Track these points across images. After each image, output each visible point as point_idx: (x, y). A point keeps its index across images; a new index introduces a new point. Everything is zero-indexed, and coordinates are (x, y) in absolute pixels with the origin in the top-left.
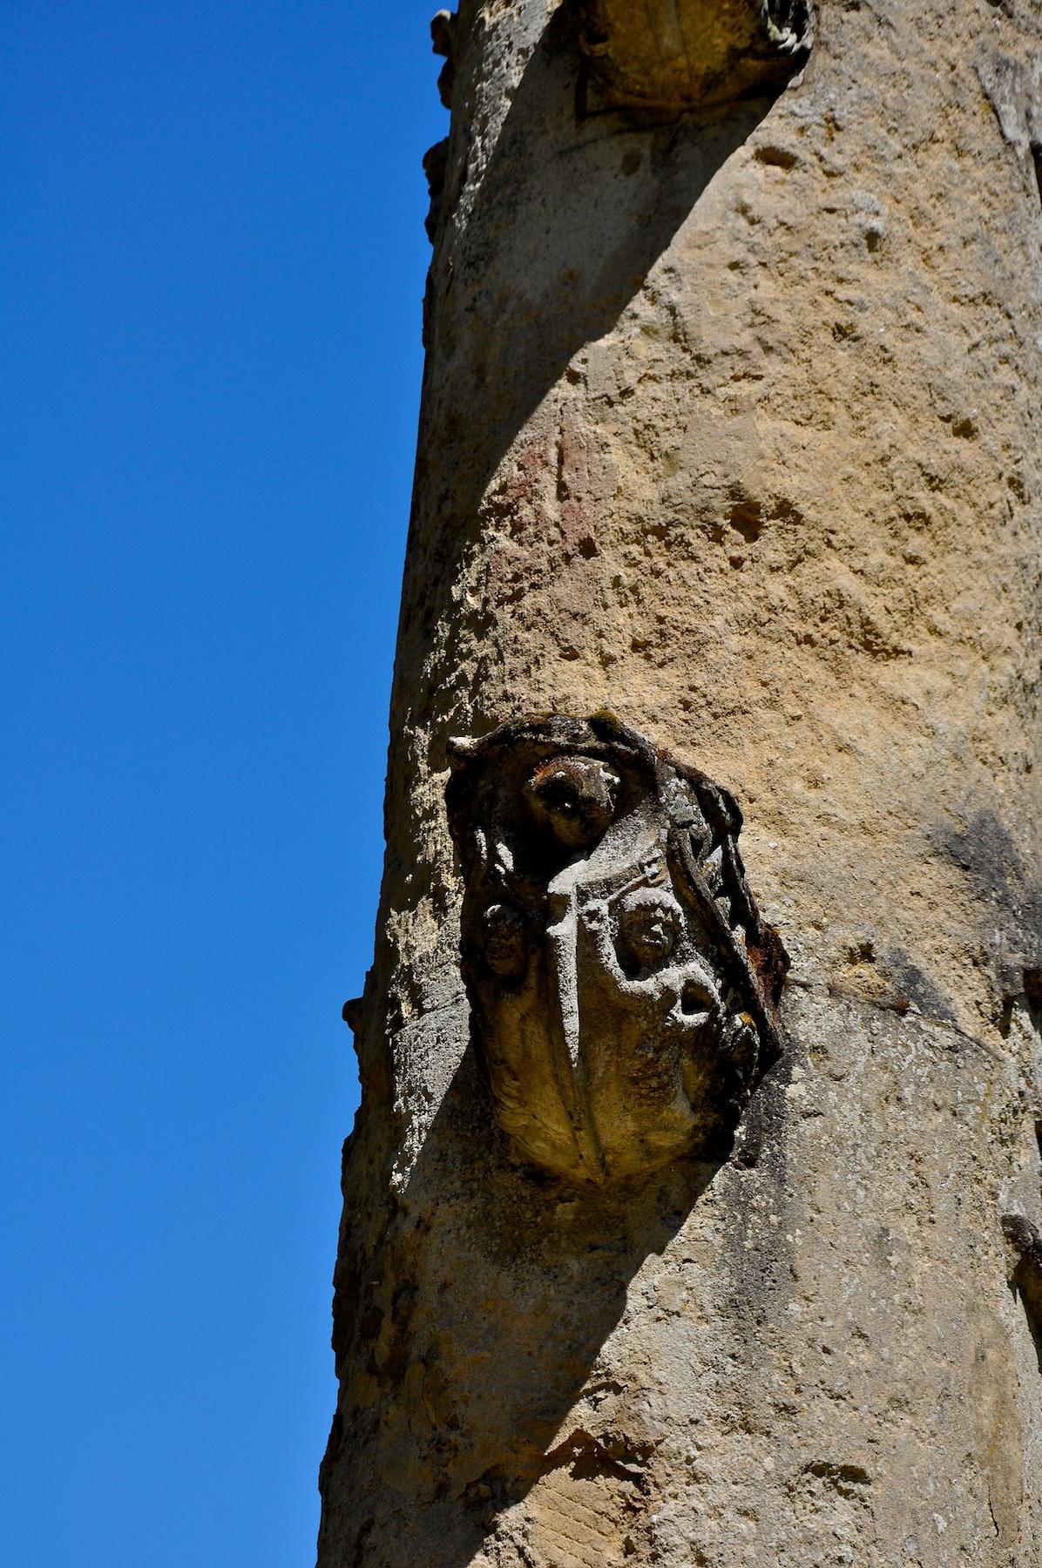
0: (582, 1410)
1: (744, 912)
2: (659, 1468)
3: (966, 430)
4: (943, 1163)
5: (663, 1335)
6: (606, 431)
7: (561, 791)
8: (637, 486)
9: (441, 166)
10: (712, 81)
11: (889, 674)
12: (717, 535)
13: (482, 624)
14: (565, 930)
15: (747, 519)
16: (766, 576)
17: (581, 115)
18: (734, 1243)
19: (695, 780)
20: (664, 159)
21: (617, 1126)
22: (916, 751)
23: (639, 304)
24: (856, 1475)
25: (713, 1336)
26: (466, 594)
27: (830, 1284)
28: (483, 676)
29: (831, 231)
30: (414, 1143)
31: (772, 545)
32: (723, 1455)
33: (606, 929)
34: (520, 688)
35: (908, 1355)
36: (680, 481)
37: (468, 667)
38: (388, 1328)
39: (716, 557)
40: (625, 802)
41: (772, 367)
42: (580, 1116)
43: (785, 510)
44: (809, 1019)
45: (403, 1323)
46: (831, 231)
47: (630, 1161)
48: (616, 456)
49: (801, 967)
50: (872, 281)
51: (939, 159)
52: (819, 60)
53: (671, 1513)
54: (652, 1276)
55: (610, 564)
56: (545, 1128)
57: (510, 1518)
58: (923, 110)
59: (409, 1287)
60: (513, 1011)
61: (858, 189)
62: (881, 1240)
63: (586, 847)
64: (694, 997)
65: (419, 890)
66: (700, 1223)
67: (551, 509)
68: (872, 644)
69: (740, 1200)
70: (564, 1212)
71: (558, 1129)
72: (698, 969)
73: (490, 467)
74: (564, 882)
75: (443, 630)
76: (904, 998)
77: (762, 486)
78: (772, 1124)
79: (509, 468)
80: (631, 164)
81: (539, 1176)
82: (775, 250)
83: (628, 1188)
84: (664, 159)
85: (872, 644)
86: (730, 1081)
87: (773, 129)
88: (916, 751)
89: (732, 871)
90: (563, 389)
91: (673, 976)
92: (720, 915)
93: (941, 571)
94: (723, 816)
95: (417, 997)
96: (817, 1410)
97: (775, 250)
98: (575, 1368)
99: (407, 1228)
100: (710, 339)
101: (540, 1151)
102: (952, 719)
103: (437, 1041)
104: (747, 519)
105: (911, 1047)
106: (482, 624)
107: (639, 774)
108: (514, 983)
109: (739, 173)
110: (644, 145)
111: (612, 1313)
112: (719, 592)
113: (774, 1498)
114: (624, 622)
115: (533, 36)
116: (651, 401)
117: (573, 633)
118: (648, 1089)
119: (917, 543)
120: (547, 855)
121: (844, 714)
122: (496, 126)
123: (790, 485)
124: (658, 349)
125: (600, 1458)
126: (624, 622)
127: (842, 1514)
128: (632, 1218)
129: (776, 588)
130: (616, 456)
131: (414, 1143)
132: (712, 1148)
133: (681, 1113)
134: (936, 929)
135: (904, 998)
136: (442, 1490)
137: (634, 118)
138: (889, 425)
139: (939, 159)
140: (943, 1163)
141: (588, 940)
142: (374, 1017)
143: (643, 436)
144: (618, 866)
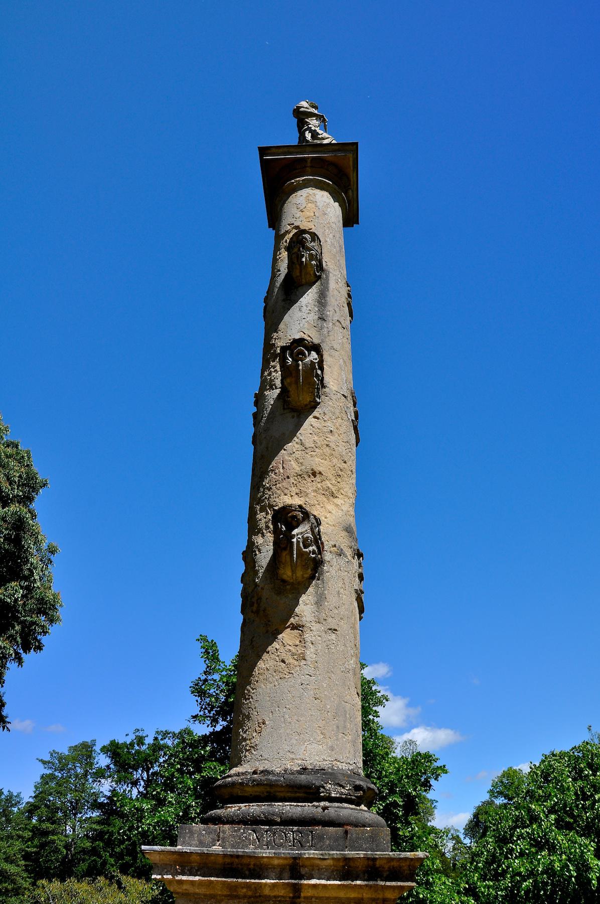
0: (292, 619)
1: (320, 539)
2: (305, 629)
3: (345, 462)
4: (347, 581)
5: (305, 607)
6: (290, 458)
7: (295, 517)
8: (295, 467)
9: (256, 417)
10: (306, 405)
11: (336, 500)
12: (309, 476)
13: (269, 489)
14: (294, 540)
15: (314, 474)
16: (317, 483)
17: (284, 409)
18: (316, 593)
19: (315, 516)
20: (299, 416)
21: (299, 573)
22: (340, 513)
23: (295, 439)
24: (336, 630)
25: (314, 608)
26: (266, 483)
27: (332, 600)
28: (270, 497)
29: (325, 430)
30: (260, 575)
31: (318, 479)
32: (315, 627)
33: (301, 540)
34: (277, 500)
35: (342, 611)
36: (303, 467)
37: (267, 496)
38: (256, 605)
39: (309, 480)
40: (304, 520)
41: (317, 450)
42: (293, 572)
43: (320, 473)
44: (327, 556)
45: (259, 605)
46: (325, 430)
47: (300, 579)
48: (292, 463)
49: (326, 548)
50: (332, 438)
51: (340, 420)
52: (322, 404)
53: (307, 636)
54: (303, 598)
55: (292, 480)
56: (286, 573)
57: (280, 636)
58: (337, 411)
59: (260, 599)
60: (284, 554)
61: (329, 424)
62: (339, 593)
63: (297, 527)
64: (314, 552)
65: (258, 532)
66: (311, 589)
67: (282, 471)
68: (333, 495)
69: (317, 586)
70: (288, 587)
71: (289, 573)
72: (314, 547)
73: (270, 464)
74: (295, 532)
75: (262, 490)
76: (340, 554)
77: (318, 469)
78: (322, 574)
79: (273, 464)
80: (293, 417)
81: (284, 581)
82: (318, 432)
83: (299, 583)
84: (299, 416)
85: (333, 495)
86: (315, 566)
87: (315, 413)
88: (340, 513)
89: (319, 531)
90: (283, 451)
91: (311, 548)
92: (317, 540)
93: (343, 485)
94: (319, 523)
95: (259, 551)
96: (330, 620)
97: (318, 432)
98: (290, 612)
99: (259, 589)
100: (307, 445)
101: (285, 577)
102: (345, 508)
103: (264, 556)
104: (314, 474)
105: (342, 561)
106: (269, 489)
107: (306, 515)
108: (285, 549)
109: (310, 420)
110: (295, 414)
111: (297, 604)
112: (310, 486)
113: (323, 634)
114: (294, 490)
115: (275, 396)
116: (298, 454)
117: (286, 491)
118: (305, 567)
119: (339, 480)
120: (291, 528)
121: (330, 507)
122: (269, 410)
123: (321, 469)
124: (298, 446)
125: (295, 627)
126: (294, 490)
127: (333, 636)
128: (300, 588)
129: (319, 485)
130: (292, 463)
131: (260, 575)
132: (312, 577)
133: (309, 571)
134: (343, 541)
135: (340, 554)
136: (267, 632)
137: (293, 410)
138: (335, 461)
139: (340, 420)
140: (347, 581)
141: (298, 542)
142: (249, 555)
143: (297, 460)
144: (301, 531)
